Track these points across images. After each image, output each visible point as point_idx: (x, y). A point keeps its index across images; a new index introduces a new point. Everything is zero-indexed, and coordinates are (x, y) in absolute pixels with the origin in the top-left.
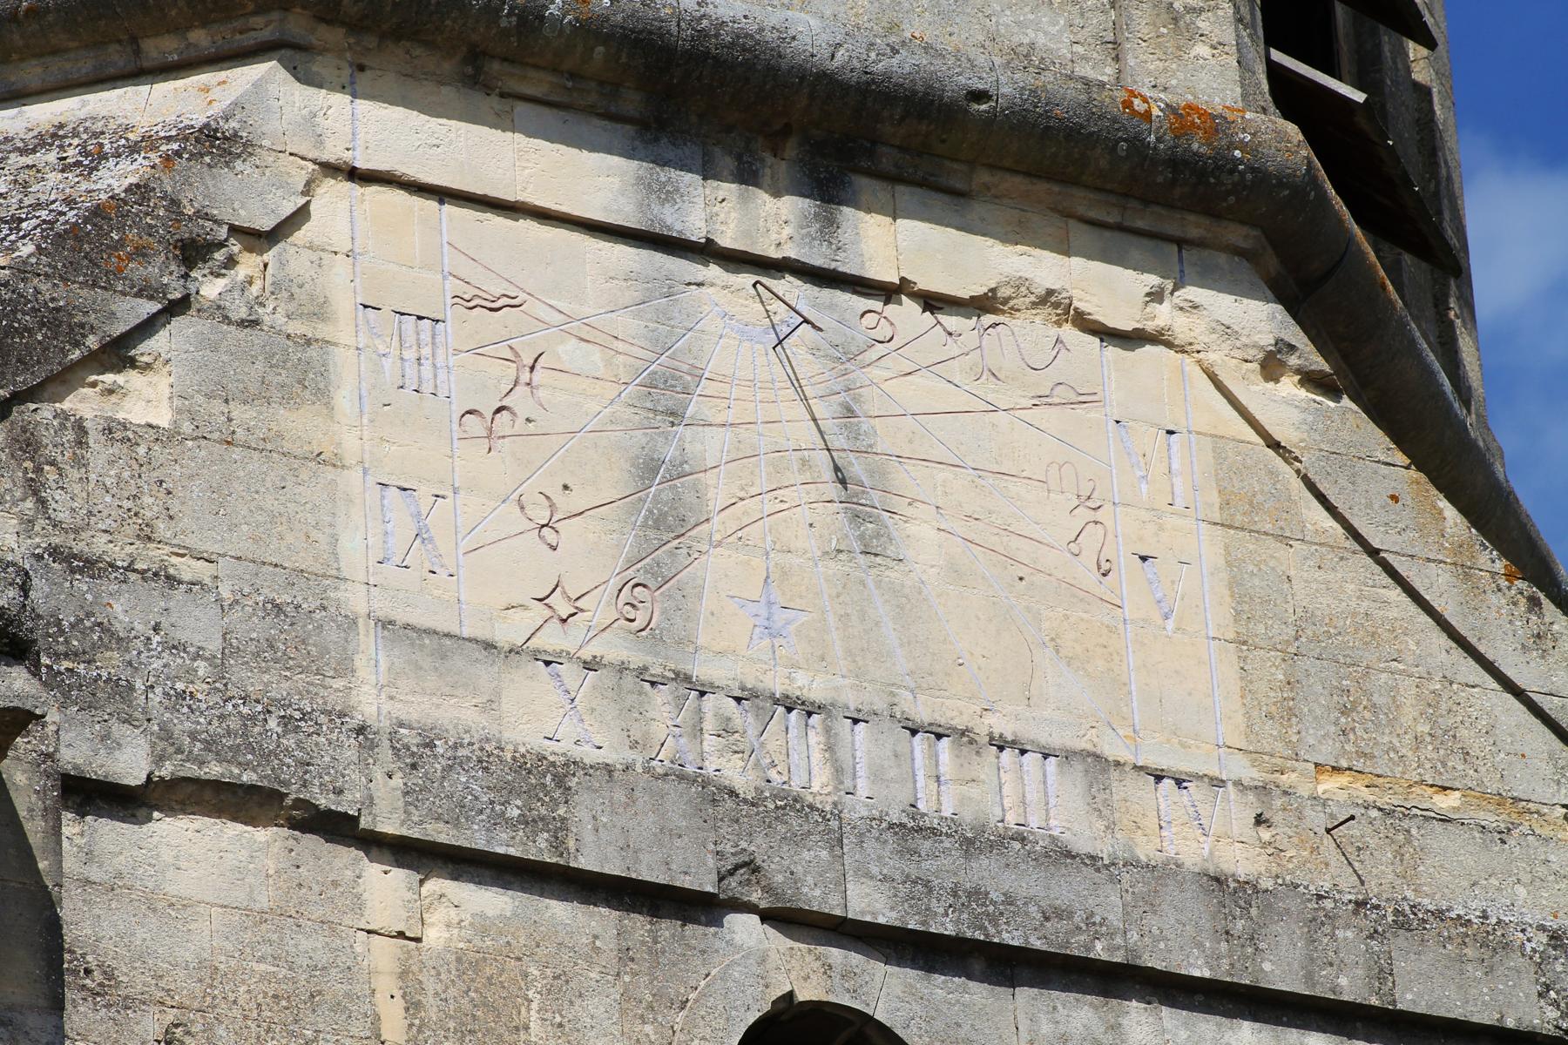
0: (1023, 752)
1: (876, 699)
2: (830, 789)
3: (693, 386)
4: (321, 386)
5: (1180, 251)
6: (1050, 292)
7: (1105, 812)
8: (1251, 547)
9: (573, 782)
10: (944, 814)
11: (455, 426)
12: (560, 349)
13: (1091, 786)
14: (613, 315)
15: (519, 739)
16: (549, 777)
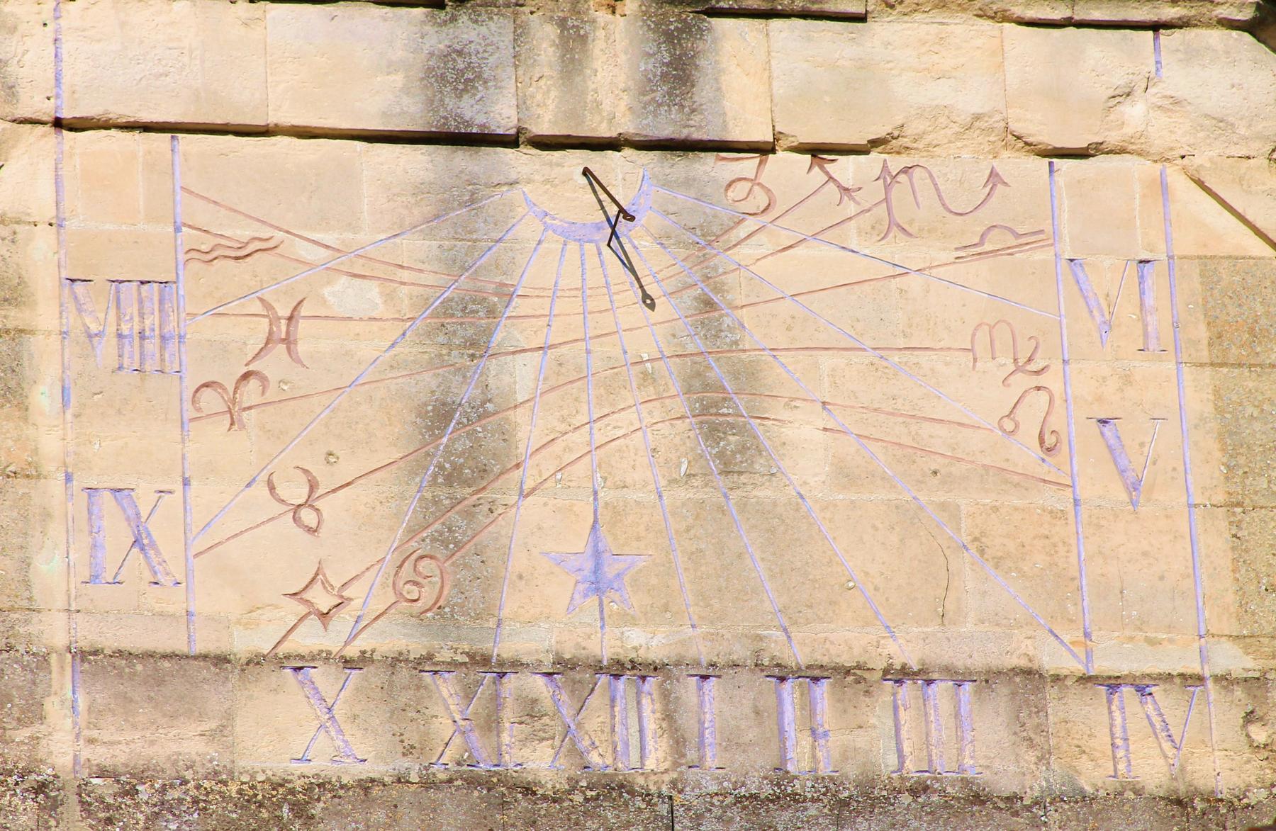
0: (929, 682)
1: (737, 647)
2: (667, 765)
3: (500, 308)
4: (12, 384)
5: (1156, 38)
6: (977, 117)
7: (1038, 739)
8: (1251, 384)
9: (317, 810)
10: (820, 773)
11: (187, 405)
12: (326, 291)
13: (1019, 711)
14: (397, 240)
15: (258, 766)
16: (285, 809)
